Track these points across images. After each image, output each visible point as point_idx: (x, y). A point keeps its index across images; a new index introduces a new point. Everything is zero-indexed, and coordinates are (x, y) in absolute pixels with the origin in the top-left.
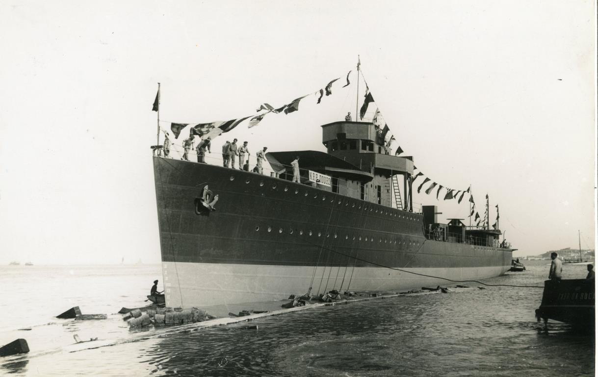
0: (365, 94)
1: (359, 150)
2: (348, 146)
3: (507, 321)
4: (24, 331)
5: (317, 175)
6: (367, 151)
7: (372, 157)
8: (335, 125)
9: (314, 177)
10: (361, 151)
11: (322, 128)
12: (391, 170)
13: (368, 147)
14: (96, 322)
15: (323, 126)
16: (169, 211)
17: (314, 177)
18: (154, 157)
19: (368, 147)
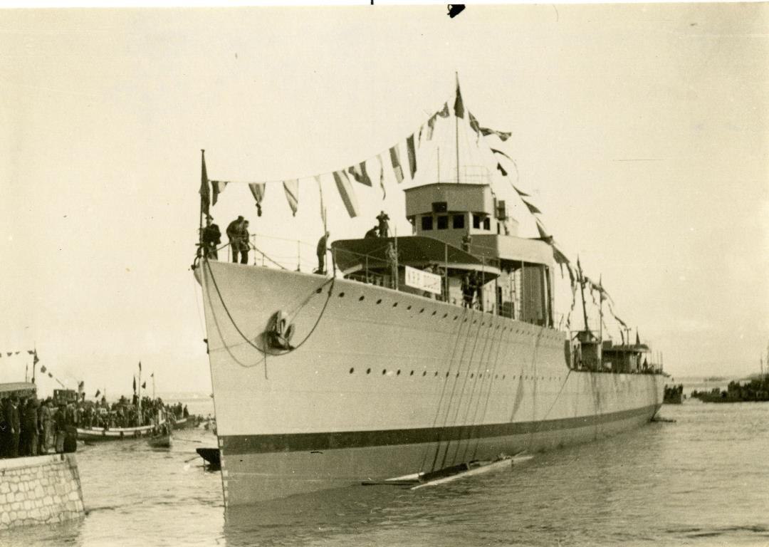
0: (193, 264)
1: (468, 229)
2: (451, 224)
3: (689, 526)
4: (320, 206)
5: (418, 274)
6: (481, 231)
7: (492, 240)
8: (431, 190)
9: (414, 278)
10: (473, 231)
11: (404, 194)
12: (443, 244)
13: (482, 224)
14: (323, 202)
15: (406, 191)
16: (16, 454)
17: (414, 278)
18: (201, 229)
19: (482, 224)
